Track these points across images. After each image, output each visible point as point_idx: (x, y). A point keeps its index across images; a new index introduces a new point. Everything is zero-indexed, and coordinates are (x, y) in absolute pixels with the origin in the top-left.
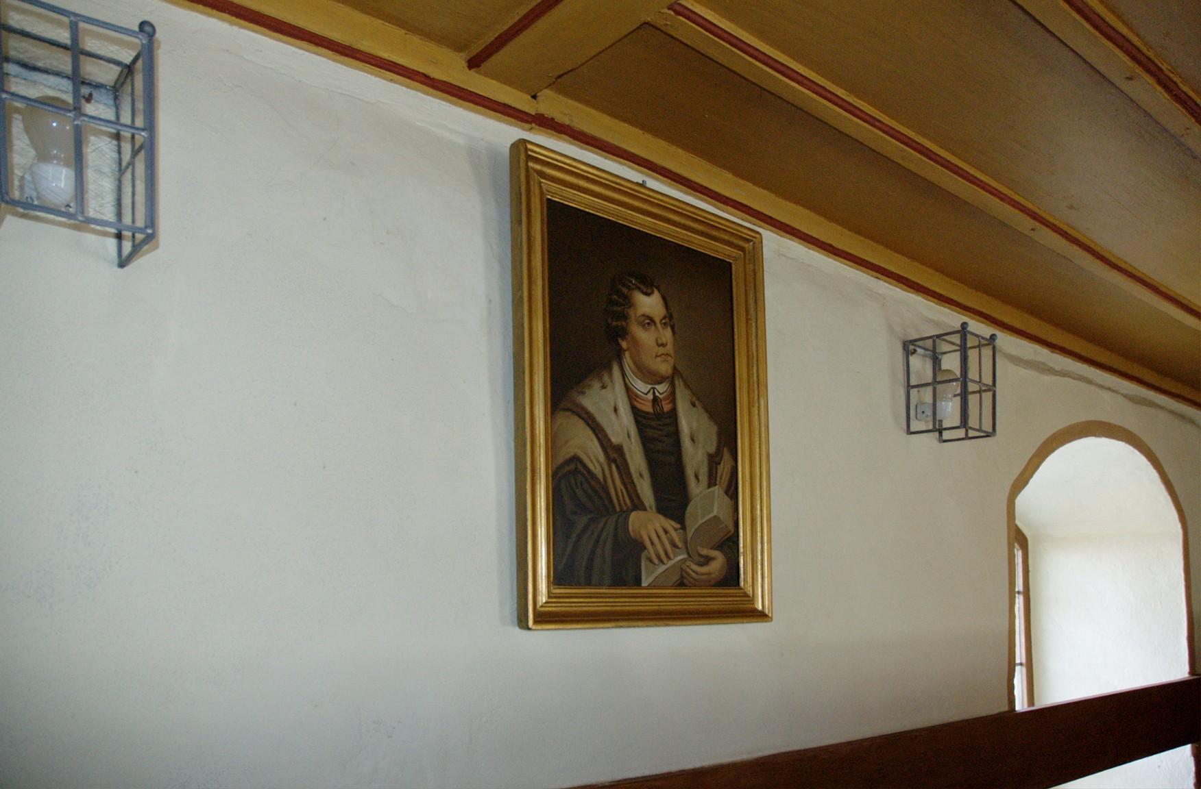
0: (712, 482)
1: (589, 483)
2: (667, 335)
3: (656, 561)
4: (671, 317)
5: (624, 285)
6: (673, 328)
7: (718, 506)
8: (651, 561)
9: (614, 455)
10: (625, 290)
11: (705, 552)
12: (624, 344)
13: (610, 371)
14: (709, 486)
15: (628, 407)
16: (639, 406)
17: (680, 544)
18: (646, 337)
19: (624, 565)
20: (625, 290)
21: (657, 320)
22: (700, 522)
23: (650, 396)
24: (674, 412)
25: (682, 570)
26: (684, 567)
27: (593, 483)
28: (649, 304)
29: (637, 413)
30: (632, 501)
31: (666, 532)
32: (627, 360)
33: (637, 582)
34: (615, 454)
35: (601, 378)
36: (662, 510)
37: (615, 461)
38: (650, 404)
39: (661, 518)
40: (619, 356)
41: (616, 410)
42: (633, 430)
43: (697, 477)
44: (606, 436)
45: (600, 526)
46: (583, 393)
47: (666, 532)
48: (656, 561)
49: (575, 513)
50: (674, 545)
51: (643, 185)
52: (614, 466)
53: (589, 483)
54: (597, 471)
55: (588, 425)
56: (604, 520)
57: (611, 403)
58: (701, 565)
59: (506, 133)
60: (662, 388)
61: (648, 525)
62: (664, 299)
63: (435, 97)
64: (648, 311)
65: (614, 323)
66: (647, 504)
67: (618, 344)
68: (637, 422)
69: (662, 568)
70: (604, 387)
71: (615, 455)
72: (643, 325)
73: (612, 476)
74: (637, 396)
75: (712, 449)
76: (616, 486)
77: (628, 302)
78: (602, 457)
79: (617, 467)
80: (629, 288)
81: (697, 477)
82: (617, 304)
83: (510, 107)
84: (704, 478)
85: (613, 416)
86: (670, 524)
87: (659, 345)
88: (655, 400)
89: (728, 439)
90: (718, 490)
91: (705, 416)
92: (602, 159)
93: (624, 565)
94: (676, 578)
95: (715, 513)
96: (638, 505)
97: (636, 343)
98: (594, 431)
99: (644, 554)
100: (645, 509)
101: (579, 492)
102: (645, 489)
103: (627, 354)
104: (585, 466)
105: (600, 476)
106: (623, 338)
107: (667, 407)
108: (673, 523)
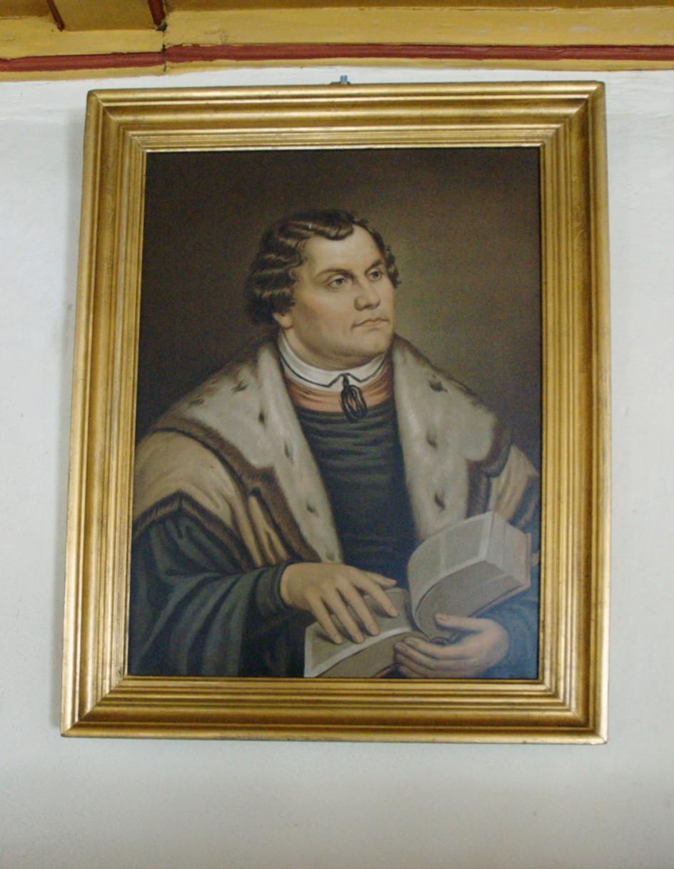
0: (476, 501)
1: (203, 529)
2: (383, 287)
3: (244, 564)
4: (390, 261)
5: (288, 236)
6: (393, 279)
7: (493, 540)
8: (326, 638)
9: (252, 484)
10: (291, 242)
11: (451, 621)
12: (285, 320)
13: (255, 362)
14: (469, 514)
15: (289, 413)
16: (305, 403)
17: (393, 612)
18: (331, 304)
19: (272, 644)
20: (291, 242)
21: (359, 273)
22: (444, 573)
23: (339, 387)
24: (389, 409)
25: (396, 651)
26: (400, 646)
27: (211, 528)
28: (353, 250)
29: (309, 421)
30: (287, 546)
31: (361, 592)
32: (291, 344)
33: (296, 670)
34: (259, 484)
35: (235, 377)
36: (353, 556)
37: (256, 493)
38: (337, 400)
39: (353, 572)
40: (273, 338)
41: (262, 418)
42: (298, 443)
43: (439, 502)
44: (238, 456)
45: (220, 592)
46: (199, 402)
47: (361, 592)
48: (338, 639)
49: (171, 572)
50: (379, 612)
51: (343, 83)
52: (253, 501)
53: (203, 529)
54: (222, 512)
55: (207, 446)
56: (229, 581)
57: (256, 414)
58: (441, 642)
59: (67, 97)
60: (363, 375)
61: (325, 584)
62: (377, 239)
63: (24, 80)
64: (340, 263)
65: (267, 294)
66: (321, 552)
67: (277, 323)
68: (308, 432)
69: (354, 648)
70: (240, 388)
71: (258, 484)
72: (327, 285)
73: (250, 516)
74: (309, 392)
75: (480, 451)
76: (257, 530)
77: (296, 256)
78: (230, 489)
79: (262, 502)
80: (302, 238)
81: (439, 502)
82: (274, 265)
83: (121, 54)
84: (457, 497)
85: (256, 427)
86: (371, 581)
87: (359, 309)
88: (348, 391)
89: (522, 425)
90: (492, 523)
91: (464, 402)
92: (297, 70)
93: (272, 644)
94: (385, 662)
95: (482, 555)
96: (300, 552)
97: (310, 314)
98: (216, 453)
99: (310, 631)
100: (315, 558)
101: (183, 543)
102: (319, 530)
103: (291, 334)
104: (195, 505)
105: (227, 520)
106: (282, 312)
107: (372, 400)
108: (380, 579)
